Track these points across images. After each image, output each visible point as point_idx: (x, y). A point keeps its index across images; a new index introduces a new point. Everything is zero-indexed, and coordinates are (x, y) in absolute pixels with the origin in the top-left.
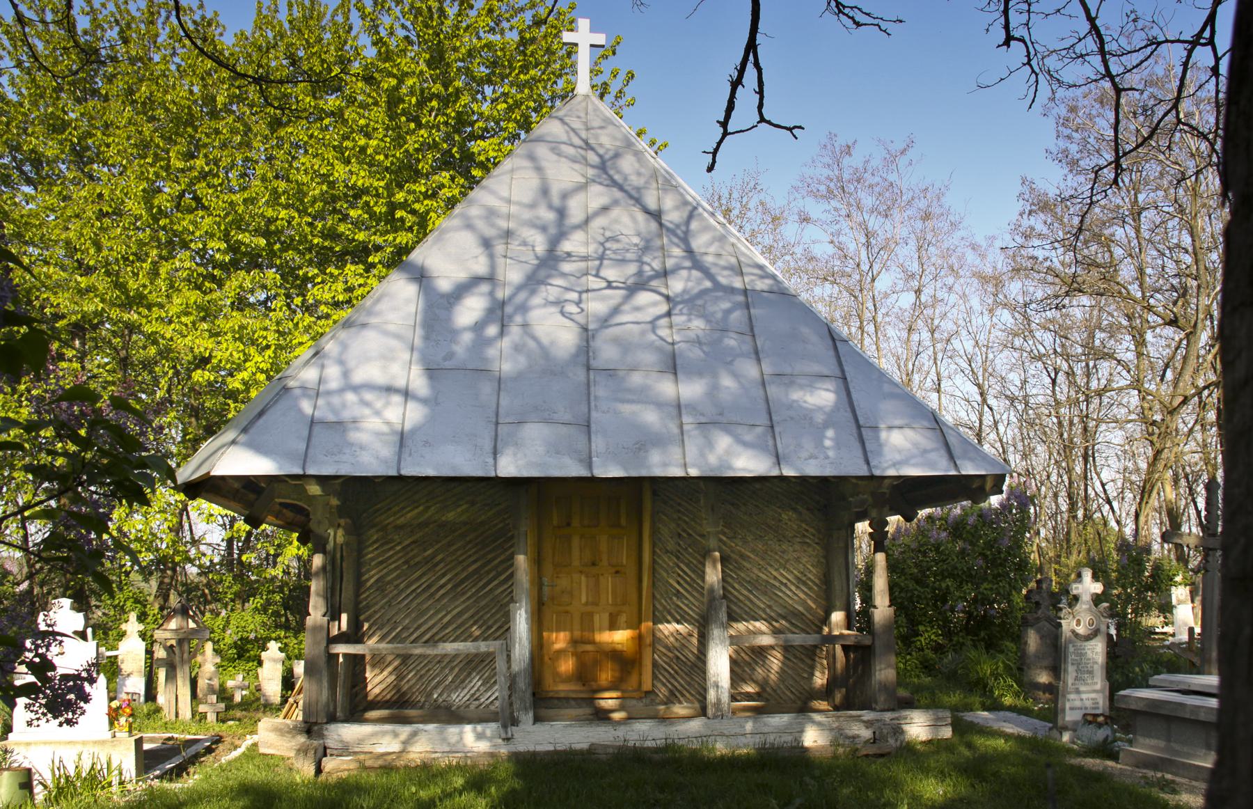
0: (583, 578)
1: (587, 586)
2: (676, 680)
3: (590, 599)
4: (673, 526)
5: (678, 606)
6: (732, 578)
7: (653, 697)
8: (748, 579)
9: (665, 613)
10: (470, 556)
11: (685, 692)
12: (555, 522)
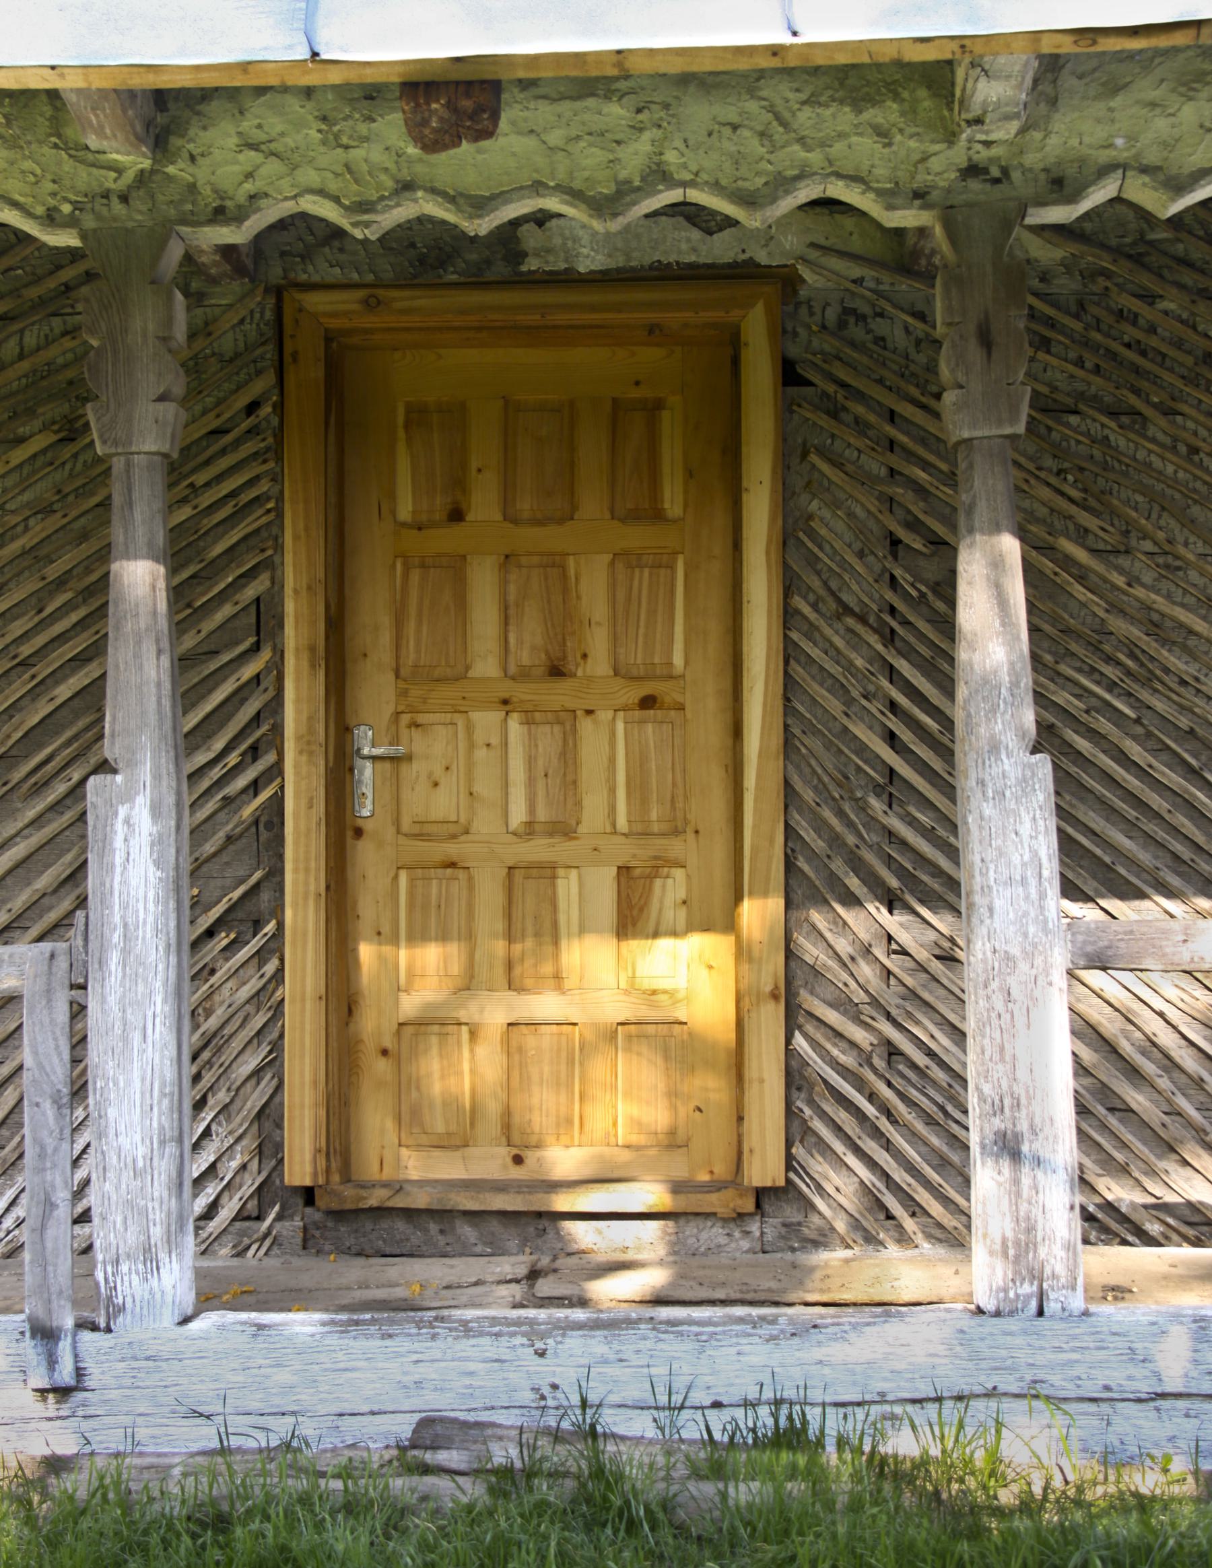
0: (515, 726)
1: (531, 761)
2: (888, 1145)
3: (542, 815)
4: (865, 503)
5: (891, 834)
6: (1117, 717)
7: (792, 1214)
8: (1184, 722)
9: (838, 866)
10: (61, 638)
11: (923, 1196)
12: (405, 511)
